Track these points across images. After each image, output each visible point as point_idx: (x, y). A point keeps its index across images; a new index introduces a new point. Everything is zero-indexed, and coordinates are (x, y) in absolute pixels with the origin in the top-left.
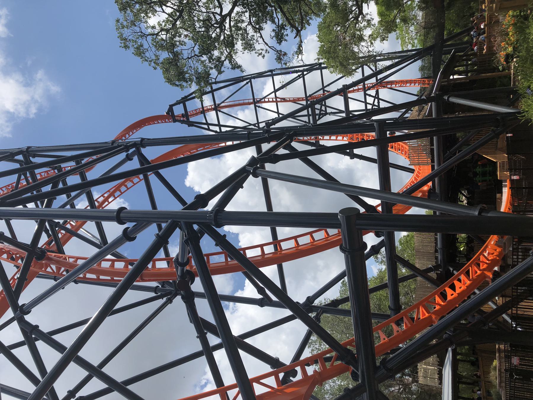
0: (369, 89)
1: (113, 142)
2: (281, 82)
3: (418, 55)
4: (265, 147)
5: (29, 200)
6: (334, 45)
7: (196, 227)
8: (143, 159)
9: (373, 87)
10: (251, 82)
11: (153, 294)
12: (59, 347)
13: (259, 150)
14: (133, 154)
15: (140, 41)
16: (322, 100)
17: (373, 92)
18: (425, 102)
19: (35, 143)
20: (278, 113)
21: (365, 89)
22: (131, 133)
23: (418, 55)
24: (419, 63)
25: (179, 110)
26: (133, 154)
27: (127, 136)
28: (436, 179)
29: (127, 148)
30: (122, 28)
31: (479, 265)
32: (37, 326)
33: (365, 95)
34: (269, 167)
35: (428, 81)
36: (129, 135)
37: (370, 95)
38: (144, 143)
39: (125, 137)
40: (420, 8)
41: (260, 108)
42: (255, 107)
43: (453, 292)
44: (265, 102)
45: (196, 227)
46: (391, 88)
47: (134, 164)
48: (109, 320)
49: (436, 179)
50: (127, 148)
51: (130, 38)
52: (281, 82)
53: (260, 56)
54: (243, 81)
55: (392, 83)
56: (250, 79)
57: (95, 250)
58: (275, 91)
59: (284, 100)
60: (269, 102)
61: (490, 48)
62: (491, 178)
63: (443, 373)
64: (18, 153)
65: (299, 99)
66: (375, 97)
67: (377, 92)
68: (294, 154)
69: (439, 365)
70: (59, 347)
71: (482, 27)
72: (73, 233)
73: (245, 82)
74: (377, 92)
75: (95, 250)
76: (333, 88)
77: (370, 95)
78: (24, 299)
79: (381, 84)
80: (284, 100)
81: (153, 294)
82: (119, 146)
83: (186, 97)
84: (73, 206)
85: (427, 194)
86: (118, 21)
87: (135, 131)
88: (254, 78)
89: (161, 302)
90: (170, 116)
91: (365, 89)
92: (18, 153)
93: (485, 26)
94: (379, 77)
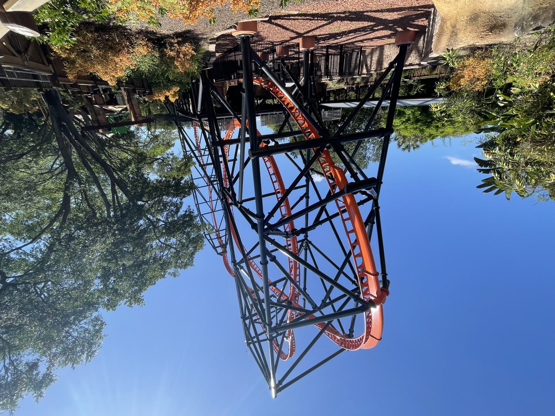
0: (201, 154)
1: (235, 276)
3: (180, 130)
4: (230, 201)
5: (262, 307)
7: (266, 227)
8: (242, 261)
9: (200, 152)
10: (202, 215)
11: (308, 251)
12: (331, 288)
13: (231, 204)
14: (240, 266)
16: (209, 178)
17: (203, 152)
18: (202, 123)
19: (239, 315)
20: (218, 199)
21: (201, 156)
23: (180, 130)
24: (185, 128)
25: (220, 250)
26: (240, 266)
28: (239, 116)
29: (237, 269)
32: (322, 301)
33: (204, 155)
34: (237, 198)
35: (361, 114)
37: (204, 153)
38: (234, 261)
41: (273, 263)
42: (215, 211)
44: (212, 207)
45: (266, 227)
46: (200, 143)
47: (244, 265)
48: (320, 269)
49: (239, 116)
50: (237, 269)
54: (202, 219)
55: (197, 143)
56: (201, 215)
57: (289, 282)
58: (206, 202)
59: (210, 197)
60: (212, 205)
64: (245, 323)
65: (209, 189)
66: (205, 150)
67: (202, 149)
68: (231, 188)
70: (331, 288)
72: (282, 293)
73: (203, 218)
74: (202, 149)
75: (289, 282)
76: (203, 173)
77: (204, 153)
78: (309, 307)
79: (198, 148)
80: (210, 197)
81: (308, 251)
82: (236, 273)
83: (213, 247)
84: (262, 287)
88: (200, 213)
89: (311, 247)
90: (223, 253)
91: (201, 156)
92: (245, 323)
94: (194, 149)
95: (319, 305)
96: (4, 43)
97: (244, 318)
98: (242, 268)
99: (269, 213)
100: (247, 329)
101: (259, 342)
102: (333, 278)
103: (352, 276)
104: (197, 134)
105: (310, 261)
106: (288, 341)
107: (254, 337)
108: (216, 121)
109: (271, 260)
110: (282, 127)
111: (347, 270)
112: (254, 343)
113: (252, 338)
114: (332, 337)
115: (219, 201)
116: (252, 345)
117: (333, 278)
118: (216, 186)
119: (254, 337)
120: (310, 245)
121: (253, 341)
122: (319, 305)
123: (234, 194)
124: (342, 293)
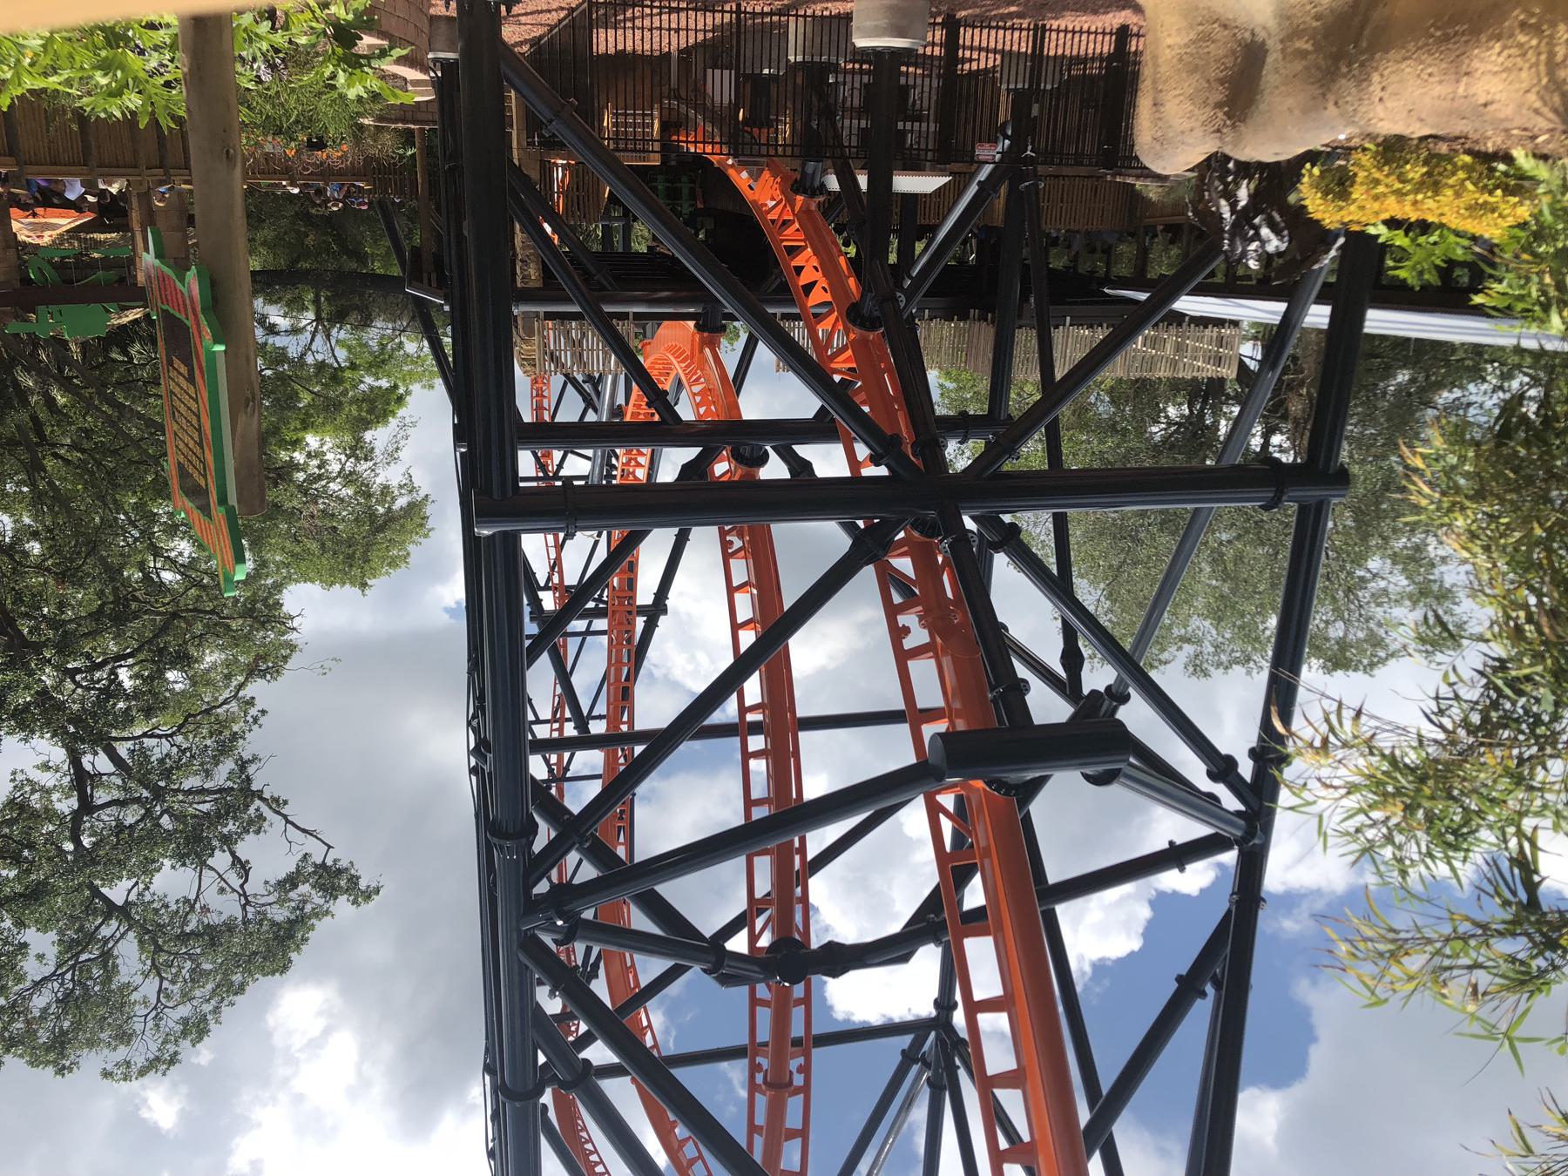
2: (321, 671)
6: (329, 544)
15: (171, 1024)
22: (589, 1146)
27: (594, 1158)
28: (608, 309)
30: (128, 1067)
31: (785, 222)
36: (591, 1153)
39: (597, 1164)
40: (366, 323)
43: (817, 288)
49: (608, 309)
51: (154, 1047)
52: (321, 671)
53: (262, 720)
61: (357, 173)
62: (684, 179)
63: (1198, 314)
69: (1180, 325)
71: (296, 191)
85: (706, 334)
86: (107, 1074)
87: (584, 1134)
93: (293, 185)
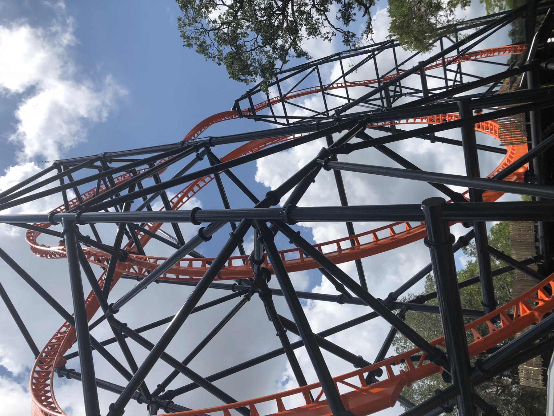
0: (450, 63)
1: (183, 143)
7: (269, 224)
9: (454, 61)
10: (317, 68)
11: (230, 292)
14: (203, 153)
17: (454, 67)
20: (348, 98)
21: (444, 65)
24: (508, 27)
25: (244, 105)
29: (196, 148)
33: (445, 70)
37: (450, 71)
38: (213, 141)
42: (323, 94)
44: (334, 88)
46: (475, 60)
47: (205, 164)
48: (191, 317)
50: (196, 148)
54: (309, 68)
55: (476, 53)
57: (174, 251)
58: (344, 75)
59: (354, 84)
60: (338, 87)
65: (370, 82)
66: (457, 72)
67: (459, 67)
73: (311, 69)
75: (174, 251)
76: (408, 66)
77: (450, 71)
78: (112, 298)
80: (354, 84)
81: (230, 292)
83: (251, 90)
88: (321, 63)
89: (239, 299)
90: (237, 112)
91: (444, 65)
95: (116, 316)
96: (429, 134)
97: (106, 158)
98: (199, 158)
99: (299, 232)
100: (89, 163)
101: (62, 189)
102: (167, 351)
103: (172, 387)
104: (496, 54)
105: (210, 295)
106: (56, 248)
107: (71, 178)
108: (524, 110)
109: (201, 230)
110: (501, 255)
111: (182, 380)
112: (59, 177)
113: (68, 173)
114: (61, 333)
115: (346, 101)
116: (55, 172)
117: (167, 351)
118: (431, 42)
119: (71, 178)
120: (167, 389)
121: (64, 174)
122: (116, 316)
123: (349, 149)
124: (139, 363)
